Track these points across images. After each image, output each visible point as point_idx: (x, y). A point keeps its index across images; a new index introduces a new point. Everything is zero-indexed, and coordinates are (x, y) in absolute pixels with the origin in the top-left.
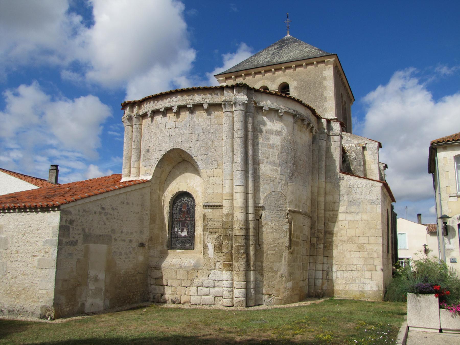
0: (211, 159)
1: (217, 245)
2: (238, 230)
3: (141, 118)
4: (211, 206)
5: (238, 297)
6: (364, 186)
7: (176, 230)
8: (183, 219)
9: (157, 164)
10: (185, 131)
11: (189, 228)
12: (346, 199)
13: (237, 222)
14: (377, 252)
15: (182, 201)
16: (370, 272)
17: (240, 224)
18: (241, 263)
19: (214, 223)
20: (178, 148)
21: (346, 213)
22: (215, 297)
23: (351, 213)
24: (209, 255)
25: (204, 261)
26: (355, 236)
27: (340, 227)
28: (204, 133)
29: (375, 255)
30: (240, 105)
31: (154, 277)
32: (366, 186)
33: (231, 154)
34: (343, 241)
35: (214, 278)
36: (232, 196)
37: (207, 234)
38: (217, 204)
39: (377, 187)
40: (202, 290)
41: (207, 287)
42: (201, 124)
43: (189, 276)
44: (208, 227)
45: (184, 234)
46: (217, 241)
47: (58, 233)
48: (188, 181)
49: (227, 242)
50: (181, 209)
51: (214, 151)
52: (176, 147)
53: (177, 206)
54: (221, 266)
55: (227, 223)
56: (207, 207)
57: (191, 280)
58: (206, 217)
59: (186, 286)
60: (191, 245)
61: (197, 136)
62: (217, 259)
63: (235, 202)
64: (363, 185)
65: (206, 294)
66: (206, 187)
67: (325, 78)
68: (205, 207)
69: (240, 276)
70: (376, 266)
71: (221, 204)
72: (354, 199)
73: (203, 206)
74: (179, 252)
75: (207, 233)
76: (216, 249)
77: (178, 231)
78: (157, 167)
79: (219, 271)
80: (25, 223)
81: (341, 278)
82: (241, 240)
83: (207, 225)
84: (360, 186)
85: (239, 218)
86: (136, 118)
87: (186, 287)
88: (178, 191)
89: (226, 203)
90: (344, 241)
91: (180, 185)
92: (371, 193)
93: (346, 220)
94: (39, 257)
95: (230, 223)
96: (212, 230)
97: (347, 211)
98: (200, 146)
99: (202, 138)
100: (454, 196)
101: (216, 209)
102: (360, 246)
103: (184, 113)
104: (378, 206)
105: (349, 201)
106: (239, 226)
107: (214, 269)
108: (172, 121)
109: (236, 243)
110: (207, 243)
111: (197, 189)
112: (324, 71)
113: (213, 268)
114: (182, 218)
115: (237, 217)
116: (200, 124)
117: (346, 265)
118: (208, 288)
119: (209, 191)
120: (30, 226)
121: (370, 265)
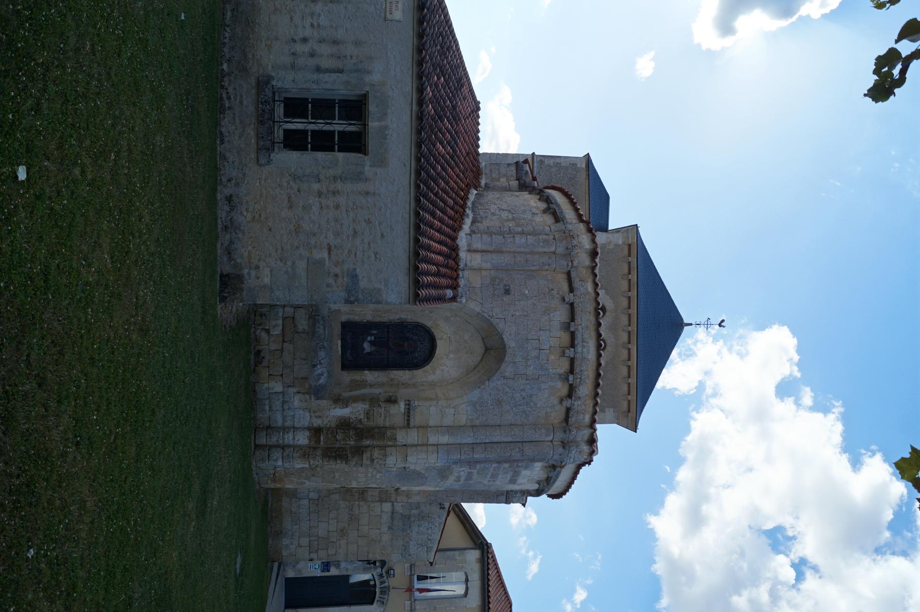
4: (409, 413)
6: (429, 537)
7: (372, 332)
9: (484, 314)
10: (532, 367)
12: (412, 513)
14: (335, 555)
16: (308, 544)
19: (383, 416)
21: (393, 513)
23: (392, 518)
24: (332, 410)
26: (359, 525)
27: (373, 505)
28: (524, 398)
29: (331, 552)
32: (429, 539)
34: (352, 508)
39: (427, 555)
45: (367, 347)
48: (452, 356)
49: (352, 438)
52: (507, 352)
53: (412, 333)
56: (407, 407)
61: (522, 387)
64: (431, 536)
67: (603, 412)
70: (317, 552)
72: (412, 524)
74: (337, 344)
75: (368, 407)
76: (341, 419)
77: (371, 335)
80: (389, 223)
81: (299, 505)
84: (430, 532)
88: (436, 338)
89: (412, 437)
90: (352, 510)
92: (419, 546)
93: (383, 513)
94: (327, 261)
97: (396, 514)
99: (518, 395)
100: (411, 571)
102: (345, 531)
104: (400, 555)
105: (409, 517)
108: (551, 342)
111: (438, 372)
112: (614, 410)
115: (391, 454)
117: (317, 511)
120: (382, 236)
121: (318, 544)
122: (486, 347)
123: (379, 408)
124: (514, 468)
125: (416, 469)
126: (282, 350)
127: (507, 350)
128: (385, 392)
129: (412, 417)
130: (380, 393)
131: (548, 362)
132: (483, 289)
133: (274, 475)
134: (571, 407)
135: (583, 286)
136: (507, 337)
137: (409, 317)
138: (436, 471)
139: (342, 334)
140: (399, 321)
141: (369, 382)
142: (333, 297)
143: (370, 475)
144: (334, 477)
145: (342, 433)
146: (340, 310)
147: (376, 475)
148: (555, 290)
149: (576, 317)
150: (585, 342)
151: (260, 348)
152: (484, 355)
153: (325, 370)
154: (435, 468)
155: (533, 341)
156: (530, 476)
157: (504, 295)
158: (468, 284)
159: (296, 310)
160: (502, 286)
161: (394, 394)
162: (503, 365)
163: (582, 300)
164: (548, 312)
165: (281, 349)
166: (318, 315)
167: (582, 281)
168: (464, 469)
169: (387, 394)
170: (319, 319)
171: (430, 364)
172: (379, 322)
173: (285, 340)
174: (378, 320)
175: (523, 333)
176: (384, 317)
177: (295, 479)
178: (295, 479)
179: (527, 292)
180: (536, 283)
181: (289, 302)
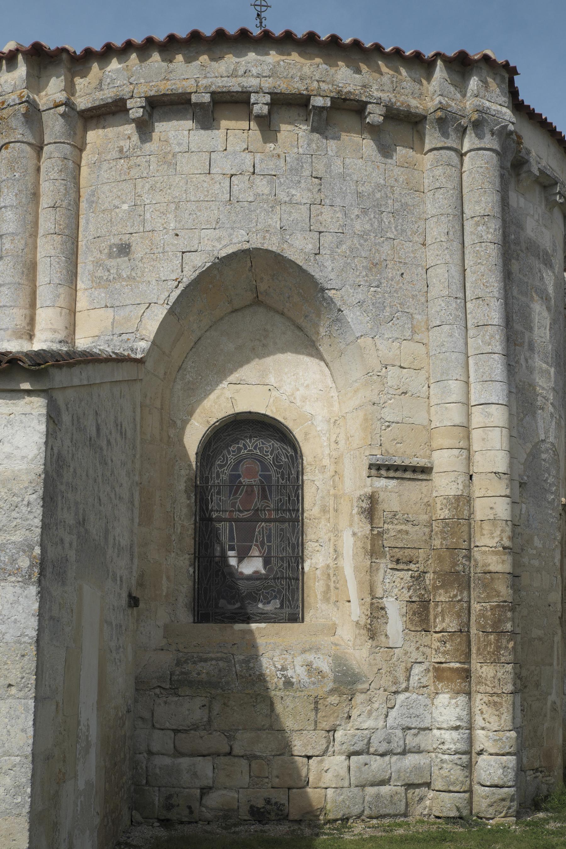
0: (391, 307)
1: (415, 606)
2: (496, 553)
3: (80, 124)
4: (397, 468)
5: (501, 783)
7: (218, 554)
8: (245, 515)
9: (172, 300)
10: (294, 192)
11: (269, 547)
13: (494, 525)
15: (239, 449)
17: (503, 535)
18: (506, 665)
19: (403, 527)
20: (270, 248)
22: (409, 786)
25: (373, 662)
28: (365, 211)
30: (493, 134)
31: (167, 725)
33: (461, 295)
35: (406, 722)
36: (468, 437)
37: (382, 565)
38: (414, 462)
40: (366, 764)
41: (382, 755)
42: (355, 178)
43: (319, 715)
44: (385, 543)
46: (415, 590)
47: (38, 511)
50: (235, 478)
51: (398, 278)
52: (259, 246)
53: (221, 466)
54: (428, 679)
55: (457, 530)
57: (328, 731)
58: (380, 507)
59: (309, 754)
60: (282, 607)
61: (339, 215)
62: (415, 656)
63: (477, 458)
65: (381, 778)
66: (376, 399)
68: (374, 472)
69: (504, 709)
71: (429, 465)
73: (371, 466)
75: (383, 561)
76: (411, 620)
78: (171, 312)
79: (420, 697)
82: (505, 587)
83: (380, 534)
85: (501, 515)
86: (63, 115)
87: (309, 757)
88: (231, 412)
91: (238, 391)
95: (465, 528)
96: (399, 554)
98: (351, 252)
99: (358, 226)
101: (410, 479)
103: (290, 127)
106: (502, 539)
107: (407, 689)
108: (238, 149)
109: (488, 596)
110: (382, 598)
111: (308, 408)
113: (404, 686)
114: (239, 511)
115: (491, 508)
116: (349, 175)
118: (387, 758)
119: (388, 415)
122: (250, 305)
123: (385, 536)
124: (522, 251)
125: (523, 461)
126: (251, 758)
127: (254, 246)
128: (351, 525)
129: (407, 463)
130: (354, 534)
131: (283, 156)
132: (117, 304)
133: (537, 770)
134: (386, 106)
135: (113, 80)
136: (225, 246)
137: (183, 472)
138: (527, 418)
139: (222, 622)
140: (193, 495)
141: (330, 561)
142: (15, 622)
143: (536, 563)
144: (540, 639)
145: (443, 620)
146: (166, 626)
147: (536, 548)
148: (122, 143)
149: (180, 91)
150: (235, 70)
151: (244, 814)
152: (269, 308)
153: (299, 660)
154: (522, 420)
155: (235, 188)
156: (537, 221)
157: (131, 256)
158: (107, 338)
159: (157, 726)
160: (112, 263)
161: (355, 504)
162: (290, 254)
163: (142, 81)
164: (170, 156)
165: (248, 759)
166: (171, 674)
167: (101, 83)
168: (522, 357)
169: (356, 518)
170: (182, 673)
171: (289, 424)
172: (195, 539)
173: (227, 749)
174: (189, 542)
175: (216, 212)
176: (183, 526)
177: (546, 725)
178: (546, 725)
179: (125, 207)
180: (106, 188)
181: (26, 757)
